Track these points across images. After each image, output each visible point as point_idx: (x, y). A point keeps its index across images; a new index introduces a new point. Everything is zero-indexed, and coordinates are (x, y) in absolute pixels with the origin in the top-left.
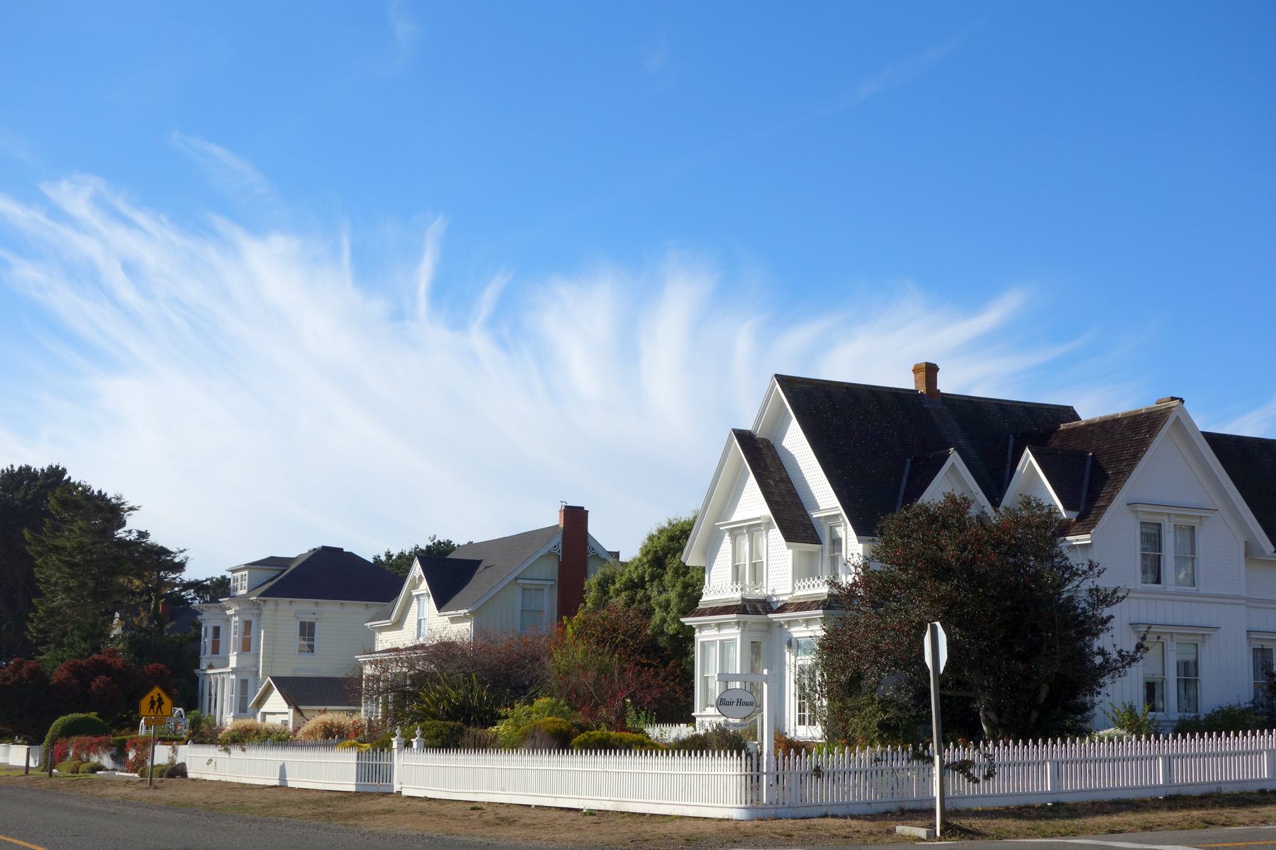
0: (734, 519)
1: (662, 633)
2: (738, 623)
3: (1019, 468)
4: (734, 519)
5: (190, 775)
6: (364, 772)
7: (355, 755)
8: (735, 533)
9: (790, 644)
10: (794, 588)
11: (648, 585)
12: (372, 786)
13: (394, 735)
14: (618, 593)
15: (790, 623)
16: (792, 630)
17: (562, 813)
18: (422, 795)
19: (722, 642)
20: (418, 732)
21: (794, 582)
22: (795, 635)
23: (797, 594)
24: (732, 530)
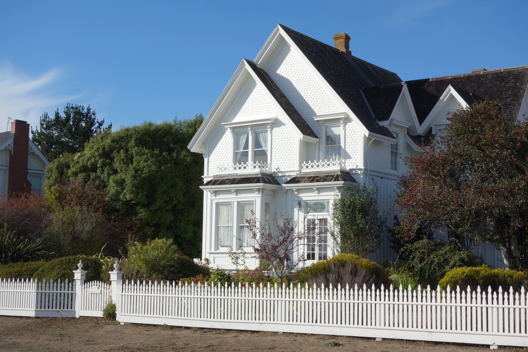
0: (234, 121)
1: (118, 200)
2: (259, 190)
3: (441, 98)
4: (234, 121)
5: (117, 319)
6: (42, 300)
7: (35, 285)
8: (239, 131)
9: (300, 204)
10: (301, 167)
11: (99, 170)
12: (52, 313)
13: (112, 269)
14: (76, 174)
15: (299, 190)
16: (301, 195)
17: (5, 318)
18: (162, 323)
19: (238, 203)
20: (80, 265)
21: (301, 162)
22: (304, 199)
23: (304, 171)
24: (253, 126)
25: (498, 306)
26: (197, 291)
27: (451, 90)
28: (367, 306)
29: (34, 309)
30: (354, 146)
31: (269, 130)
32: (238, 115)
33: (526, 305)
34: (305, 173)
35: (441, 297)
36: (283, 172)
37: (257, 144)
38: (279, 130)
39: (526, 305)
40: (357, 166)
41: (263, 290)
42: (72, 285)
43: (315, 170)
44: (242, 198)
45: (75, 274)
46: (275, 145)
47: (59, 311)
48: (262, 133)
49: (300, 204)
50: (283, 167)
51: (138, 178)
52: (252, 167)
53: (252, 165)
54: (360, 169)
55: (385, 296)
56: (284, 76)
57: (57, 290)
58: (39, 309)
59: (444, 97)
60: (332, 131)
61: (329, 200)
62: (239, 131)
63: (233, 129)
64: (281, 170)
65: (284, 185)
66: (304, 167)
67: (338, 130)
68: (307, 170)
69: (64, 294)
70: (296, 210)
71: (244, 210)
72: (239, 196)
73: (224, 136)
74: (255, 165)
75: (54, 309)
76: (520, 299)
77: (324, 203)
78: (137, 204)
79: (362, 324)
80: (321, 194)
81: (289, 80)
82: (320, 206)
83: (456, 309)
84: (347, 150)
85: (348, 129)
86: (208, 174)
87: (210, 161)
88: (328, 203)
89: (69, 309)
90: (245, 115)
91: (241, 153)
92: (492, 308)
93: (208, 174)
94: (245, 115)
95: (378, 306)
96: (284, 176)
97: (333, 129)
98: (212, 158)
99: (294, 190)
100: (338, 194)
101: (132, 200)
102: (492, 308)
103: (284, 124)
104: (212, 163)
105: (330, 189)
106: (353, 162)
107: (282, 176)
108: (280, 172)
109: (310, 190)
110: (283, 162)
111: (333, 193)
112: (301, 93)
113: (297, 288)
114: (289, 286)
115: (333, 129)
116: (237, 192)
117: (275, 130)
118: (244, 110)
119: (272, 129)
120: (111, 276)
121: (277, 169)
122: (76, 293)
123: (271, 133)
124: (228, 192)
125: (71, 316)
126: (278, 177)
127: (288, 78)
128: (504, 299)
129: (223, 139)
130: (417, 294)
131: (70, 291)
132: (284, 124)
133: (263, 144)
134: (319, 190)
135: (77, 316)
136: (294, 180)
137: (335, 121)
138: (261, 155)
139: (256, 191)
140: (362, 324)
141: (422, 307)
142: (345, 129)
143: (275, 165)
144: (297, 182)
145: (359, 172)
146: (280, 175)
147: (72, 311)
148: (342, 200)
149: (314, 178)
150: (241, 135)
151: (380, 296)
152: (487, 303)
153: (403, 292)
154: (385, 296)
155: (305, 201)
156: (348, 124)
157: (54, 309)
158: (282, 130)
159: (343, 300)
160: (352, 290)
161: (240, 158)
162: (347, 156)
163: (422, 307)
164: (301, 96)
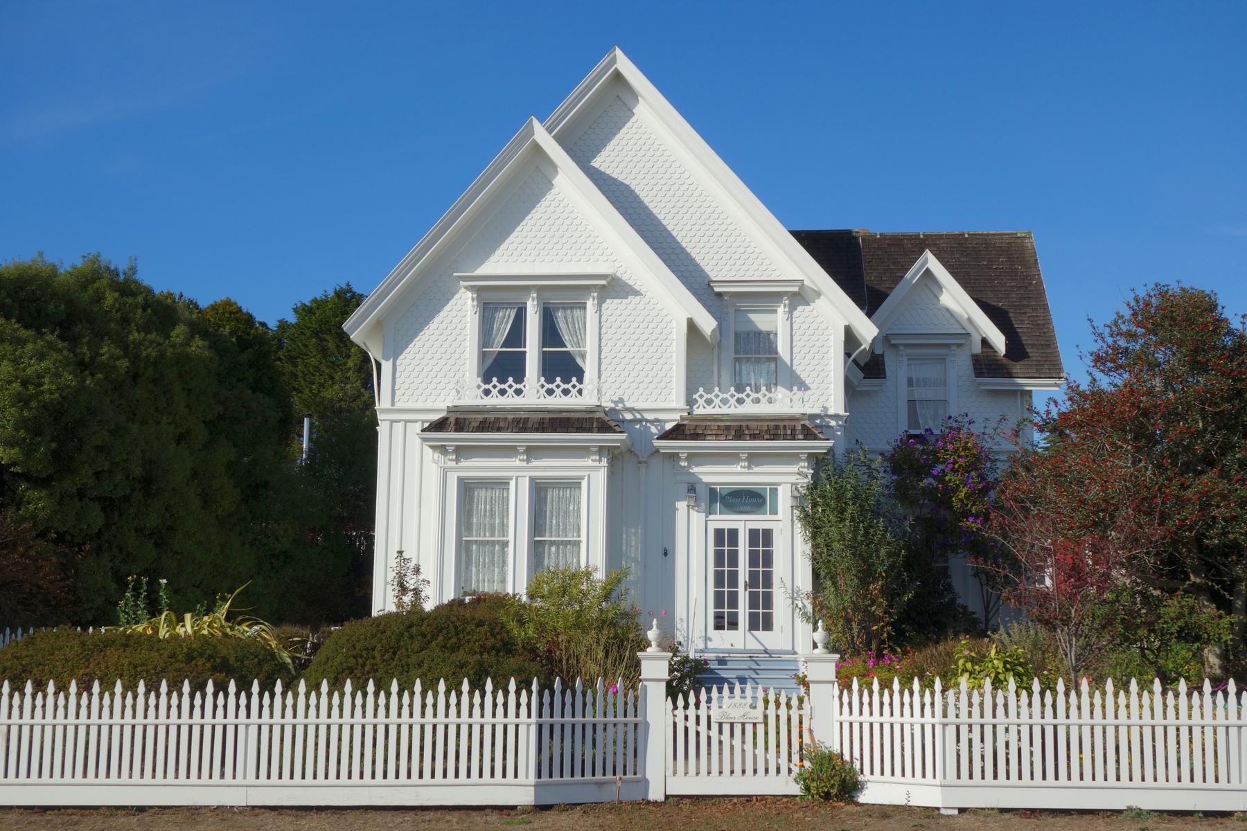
2: (601, 451)
3: (908, 275)
4: (480, 271)
8: (495, 301)
10: (690, 402)
15: (693, 458)
21: (691, 389)
22: (706, 479)
23: (699, 410)
25: (1068, 721)
26: (982, 705)
27: (931, 262)
28: (1104, 732)
29: (528, 775)
30: (815, 362)
31: (591, 304)
32: (493, 259)
33: (1239, 718)
34: (704, 418)
35: (495, 705)
36: (638, 411)
37: (550, 334)
38: (623, 306)
39: (1239, 718)
40: (825, 409)
41: (922, 696)
42: (636, 698)
43: (717, 411)
44: (546, 468)
45: (643, 663)
46: (611, 343)
47: (600, 784)
48: (565, 309)
49: (692, 489)
50: (634, 398)
51: (33, 404)
52: (543, 391)
53: (479, 387)
54: (836, 417)
55: (902, 704)
56: (615, 176)
57: (552, 716)
58: (545, 779)
59: (913, 274)
60: (751, 322)
61: (779, 484)
62: (495, 301)
63: (479, 290)
64: (628, 405)
65: (657, 443)
66: (701, 401)
67: (775, 321)
68: (709, 410)
69: (552, 726)
70: (682, 506)
71: (471, 498)
72: (464, 463)
73: (447, 308)
74: (489, 386)
75: (588, 777)
76: (458, 704)
77: (762, 493)
78: (26, 477)
79: (1044, 778)
80: (756, 469)
81: (627, 187)
82: (748, 499)
83: (271, 731)
84: (798, 369)
85: (799, 320)
86: (393, 403)
87: (399, 369)
88: (774, 492)
89: (630, 776)
90: (519, 256)
91: (493, 357)
92: (247, 726)
93: (393, 403)
94: (519, 256)
95: (241, 730)
96: (640, 421)
97: (752, 316)
98: (407, 361)
99: (683, 456)
100: (805, 470)
101: (14, 464)
102: (247, 726)
103: (637, 293)
104: (406, 374)
105: (791, 458)
106: (815, 398)
107: (635, 421)
108: (631, 410)
109: (729, 458)
110: (634, 386)
111: (794, 469)
112: (664, 222)
113: (1127, 692)
114: (1126, 686)
115: (752, 316)
116: (532, 452)
117: (610, 304)
118: (513, 247)
119: (601, 301)
120: (645, 666)
121: (616, 403)
122: (647, 725)
123: (599, 310)
124: (509, 451)
125: (629, 795)
126: (623, 421)
127: (627, 182)
128: (238, 707)
129: (442, 314)
130: (112, 701)
131: (631, 718)
132: (637, 293)
133: (566, 337)
134: (755, 459)
135: (656, 794)
136: (678, 432)
137: (767, 299)
138: (562, 367)
139: (594, 453)
140: (924, 776)
141: (1117, 731)
142: (791, 318)
143: (610, 392)
144: (695, 436)
145: (833, 423)
146: (628, 416)
147: (637, 781)
148: (814, 487)
149: (740, 429)
150: (496, 310)
151: (891, 704)
152: (1055, 716)
153: (881, 695)
154: (902, 704)
155: (707, 484)
156: (800, 308)
157: (588, 777)
158: (631, 307)
159: (1147, 718)
160: (906, 692)
161: (502, 367)
162: (795, 382)
163: (1117, 731)
164: (666, 229)
